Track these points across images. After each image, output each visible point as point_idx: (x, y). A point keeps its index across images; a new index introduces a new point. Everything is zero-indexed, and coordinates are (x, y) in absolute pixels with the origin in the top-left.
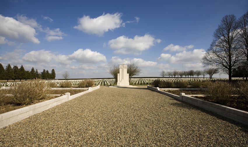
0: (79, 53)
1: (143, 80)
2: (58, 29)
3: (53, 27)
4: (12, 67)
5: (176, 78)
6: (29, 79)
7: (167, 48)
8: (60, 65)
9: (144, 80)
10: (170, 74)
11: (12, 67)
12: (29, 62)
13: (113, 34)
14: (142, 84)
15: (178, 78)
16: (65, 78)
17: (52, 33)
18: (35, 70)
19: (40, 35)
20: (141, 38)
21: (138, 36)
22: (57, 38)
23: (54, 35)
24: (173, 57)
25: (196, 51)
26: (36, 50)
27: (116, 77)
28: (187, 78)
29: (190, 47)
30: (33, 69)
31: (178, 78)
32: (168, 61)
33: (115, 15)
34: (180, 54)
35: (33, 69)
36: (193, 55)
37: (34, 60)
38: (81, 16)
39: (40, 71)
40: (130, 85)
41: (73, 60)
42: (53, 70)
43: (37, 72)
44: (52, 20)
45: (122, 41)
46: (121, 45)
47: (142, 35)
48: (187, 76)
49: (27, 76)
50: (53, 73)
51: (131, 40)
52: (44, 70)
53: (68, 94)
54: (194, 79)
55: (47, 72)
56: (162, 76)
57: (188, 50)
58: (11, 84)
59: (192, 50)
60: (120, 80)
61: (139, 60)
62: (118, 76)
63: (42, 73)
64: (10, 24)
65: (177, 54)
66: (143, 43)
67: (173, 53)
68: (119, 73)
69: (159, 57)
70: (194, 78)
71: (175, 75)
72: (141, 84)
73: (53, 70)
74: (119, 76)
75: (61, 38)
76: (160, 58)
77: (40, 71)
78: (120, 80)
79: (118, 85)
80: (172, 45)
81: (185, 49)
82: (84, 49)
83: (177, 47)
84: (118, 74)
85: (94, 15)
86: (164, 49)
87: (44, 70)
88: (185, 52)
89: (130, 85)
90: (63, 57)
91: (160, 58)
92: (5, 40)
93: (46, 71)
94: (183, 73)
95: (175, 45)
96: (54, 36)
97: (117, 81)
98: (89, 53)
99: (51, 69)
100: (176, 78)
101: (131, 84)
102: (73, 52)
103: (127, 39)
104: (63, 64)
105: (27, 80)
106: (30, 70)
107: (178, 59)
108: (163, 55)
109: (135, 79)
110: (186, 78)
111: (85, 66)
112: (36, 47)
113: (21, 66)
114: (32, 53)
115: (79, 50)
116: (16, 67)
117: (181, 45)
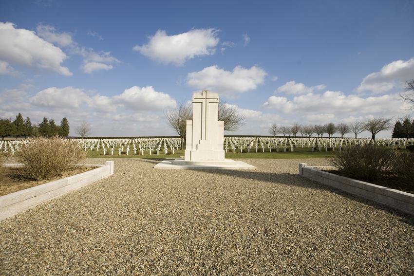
0: (133, 93)
2: (108, 54)
3: (99, 48)
5: (286, 137)
6: (10, 136)
7: (283, 88)
8: (95, 114)
10: (285, 130)
12: (42, 106)
13: (198, 63)
15: (290, 137)
16: (80, 136)
17: (97, 57)
18: (24, 118)
19: (73, 62)
20: (245, 72)
21: (242, 67)
22: (104, 66)
23: (96, 63)
24: (288, 103)
25: (328, 94)
26: (58, 87)
27: (183, 135)
28: (304, 137)
29: (320, 87)
31: (290, 137)
32: (279, 111)
33: (210, 31)
34: (301, 99)
36: (323, 101)
37: (52, 103)
38: (153, 33)
39: (36, 123)
40: (227, 157)
41: (120, 105)
42: (65, 120)
43: (28, 122)
44: (101, 38)
45: (212, 73)
46: (210, 81)
47: (248, 67)
48: (304, 135)
49: (6, 130)
50: (64, 126)
51: (227, 73)
52: (45, 120)
53: (111, 163)
54: (346, 142)
55: (52, 122)
57: (316, 92)
58: (129, 141)
59: (322, 93)
60: (196, 142)
62: (188, 129)
63: (40, 125)
64: (23, 41)
65: (295, 98)
66: (245, 79)
67: (290, 97)
68: (191, 119)
69: (265, 102)
70: (342, 140)
71: (295, 133)
73: (65, 120)
74: (193, 131)
75: (111, 67)
76: (267, 103)
77: (36, 123)
78: (196, 142)
79: (187, 159)
80: (293, 82)
81: (311, 89)
82: (142, 85)
83: (300, 87)
84: (188, 122)
85: (173, 31)
86: (279, 88)
87: (45, 120)
88: (310, 94)
89: (227, 157)
90: (103, 100)
91: (267, 103)
92: (7, 68)
93: (48, 122)
94: (314, 128)
95: (297, 82)
96: (99, 62)
97: (183, 146)
98: (149, 94)
100: (286, 137)
101: (230, 153)
102: (122, 92)
103: (222, 71)
104: (100, 111)
107: (296, 107)
108: (273, 99)
110: (302, 137)
111: (139, 117)
112: (60, 82)
114: (50, 91)
115: (136, 87)
117: (307, 84)
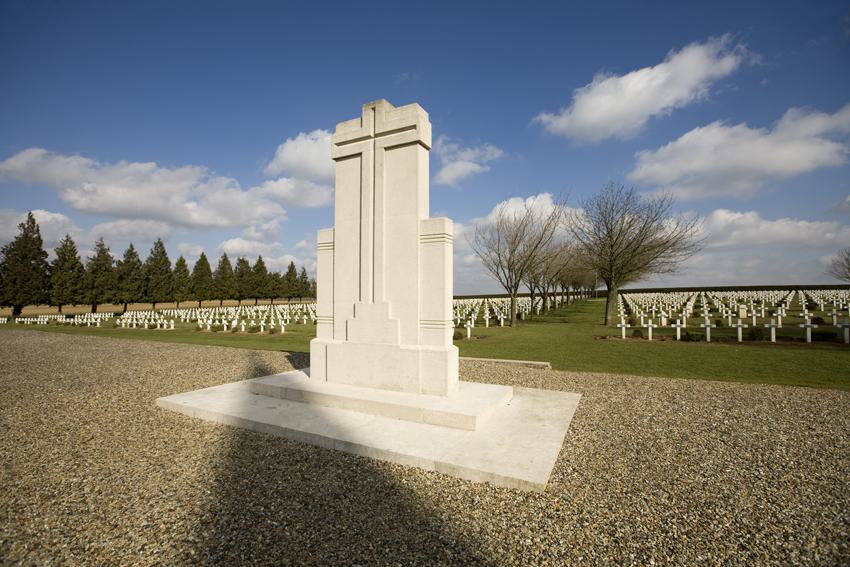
1: (710, 303)
4: (234, 263)
9: (717, 303)
11: (234, 263)
14: (703, 337)
18: (299, 271)
30: (292, 267)
35: (292, 267)
56: (840, 278)
60: (343, 313)
61: (739, 219)
72: (687, 337)
73: (160, 245)
99: (92, 241)
105: (99, 308)
106: (283, 272)
109: (672, 294)
113: (129, 247)
116: (242, 262)
